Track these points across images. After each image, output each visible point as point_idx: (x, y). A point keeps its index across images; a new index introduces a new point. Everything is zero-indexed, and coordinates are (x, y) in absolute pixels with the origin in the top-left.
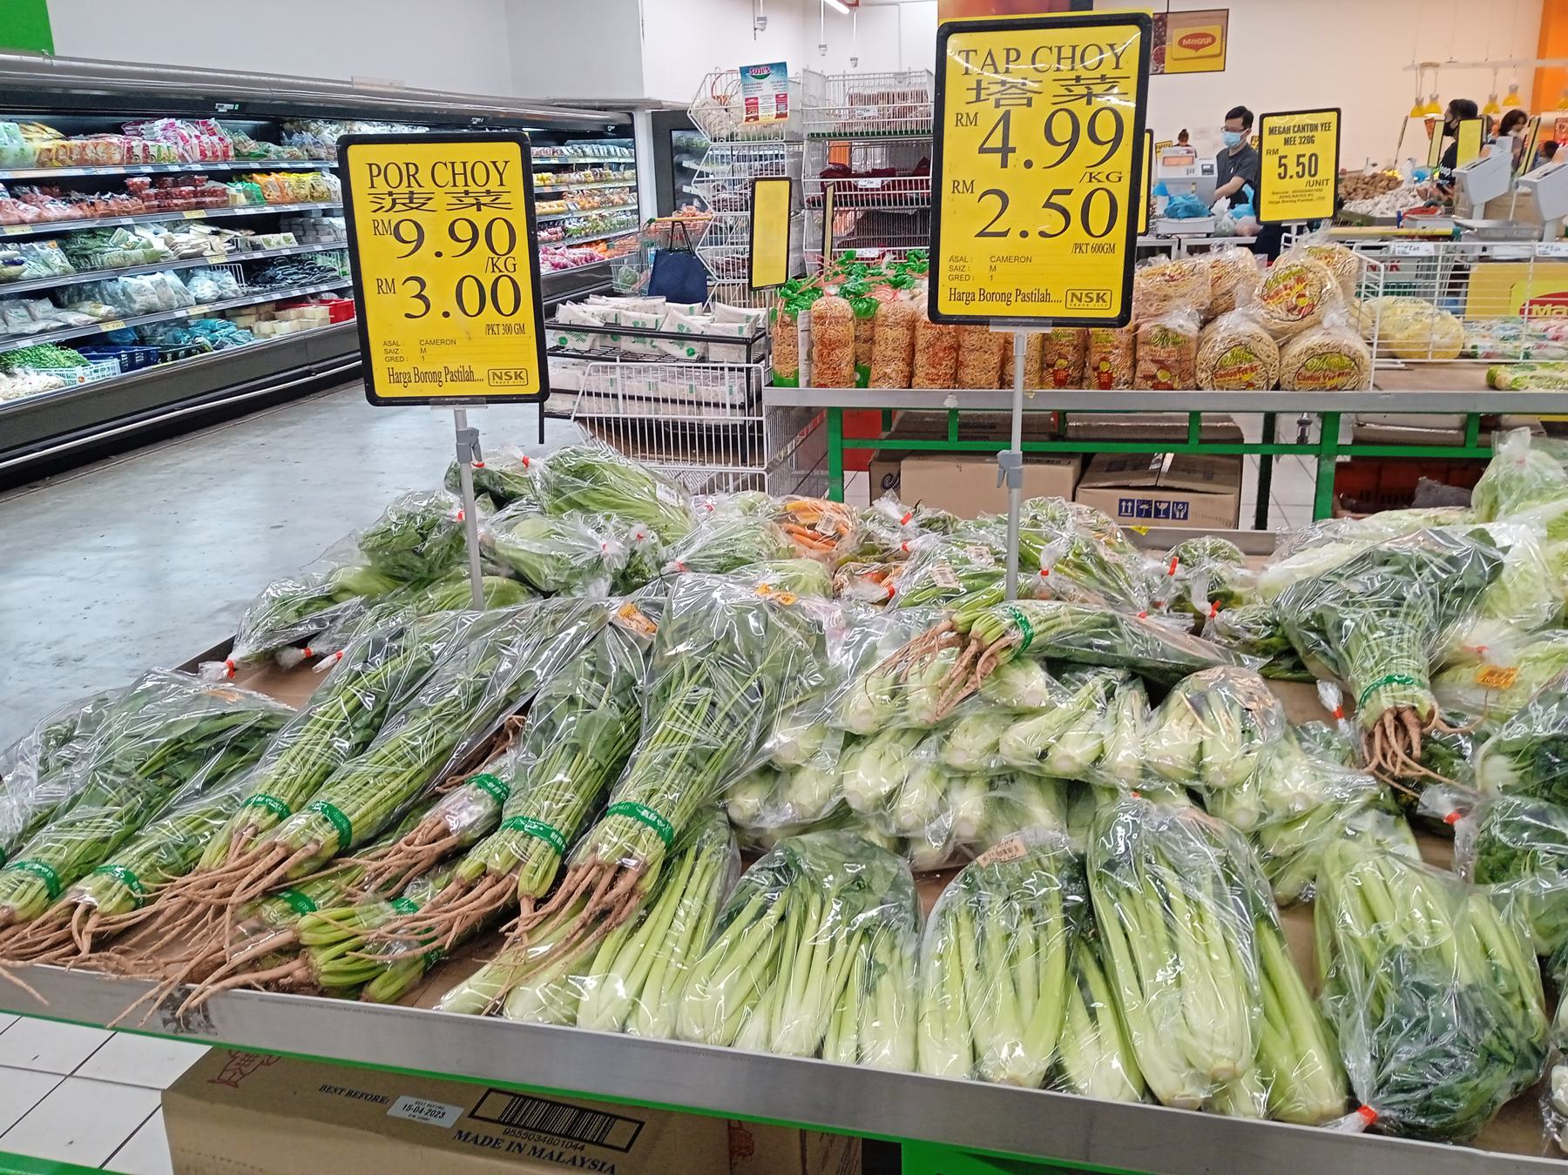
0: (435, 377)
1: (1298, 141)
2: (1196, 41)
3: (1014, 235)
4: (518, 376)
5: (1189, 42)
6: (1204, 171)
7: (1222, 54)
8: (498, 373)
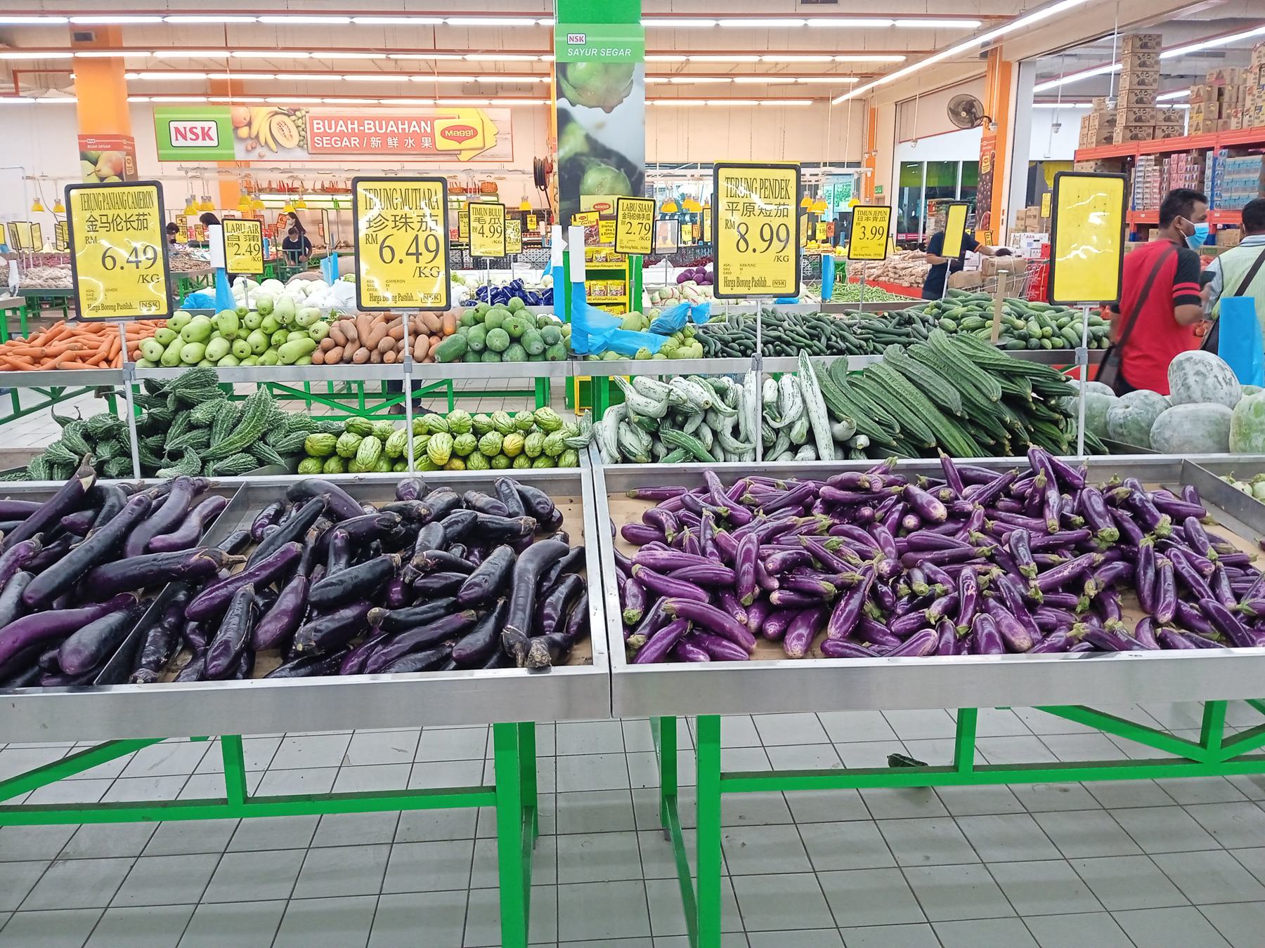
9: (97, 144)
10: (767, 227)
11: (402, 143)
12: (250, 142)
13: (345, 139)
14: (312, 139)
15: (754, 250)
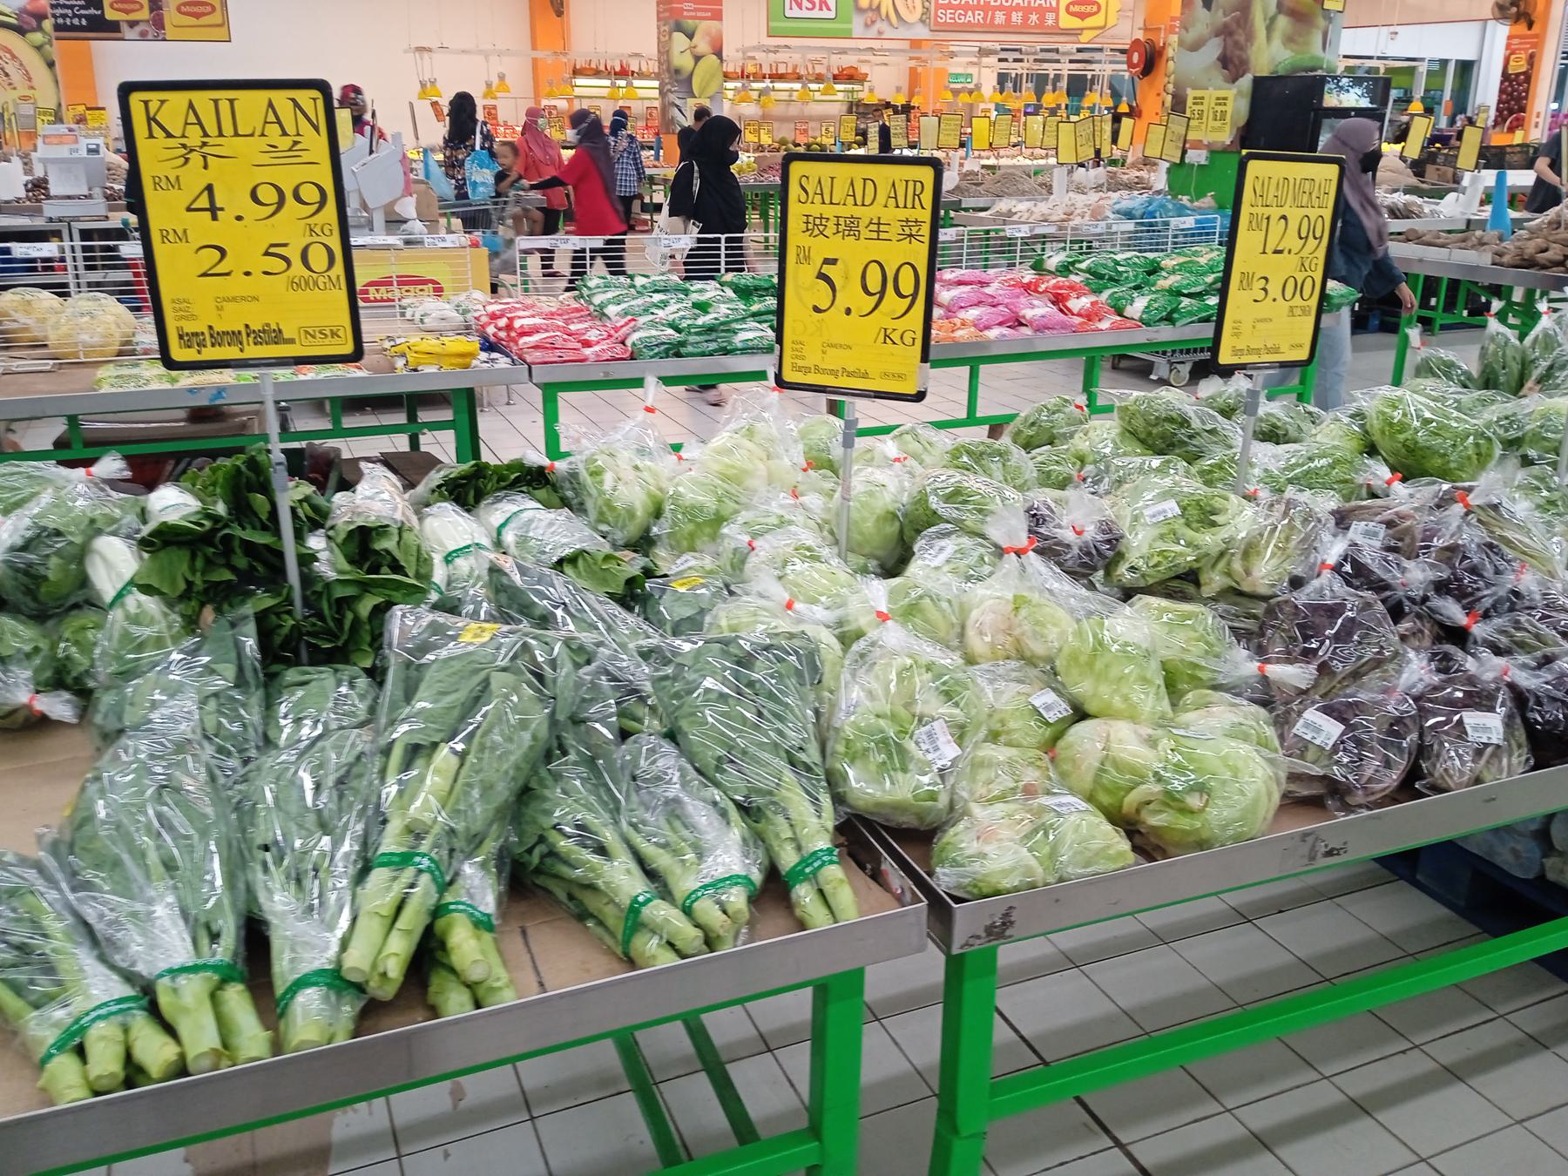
0: (234, 337)
1: (896, 228)
2: (196, 9)
3: (1286, 252)
4: (334, 334)
5: (188, 9)
6: (90, 151)
7: (225, 23)
8: (310, 330)
9: (696, 10)
10: (874, 268)
11: (1025, 19)
12: (870, 14)
13: (970, 13)
14: (936, 10)
15: (848, 311)
